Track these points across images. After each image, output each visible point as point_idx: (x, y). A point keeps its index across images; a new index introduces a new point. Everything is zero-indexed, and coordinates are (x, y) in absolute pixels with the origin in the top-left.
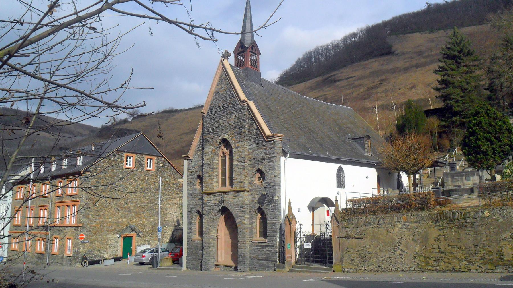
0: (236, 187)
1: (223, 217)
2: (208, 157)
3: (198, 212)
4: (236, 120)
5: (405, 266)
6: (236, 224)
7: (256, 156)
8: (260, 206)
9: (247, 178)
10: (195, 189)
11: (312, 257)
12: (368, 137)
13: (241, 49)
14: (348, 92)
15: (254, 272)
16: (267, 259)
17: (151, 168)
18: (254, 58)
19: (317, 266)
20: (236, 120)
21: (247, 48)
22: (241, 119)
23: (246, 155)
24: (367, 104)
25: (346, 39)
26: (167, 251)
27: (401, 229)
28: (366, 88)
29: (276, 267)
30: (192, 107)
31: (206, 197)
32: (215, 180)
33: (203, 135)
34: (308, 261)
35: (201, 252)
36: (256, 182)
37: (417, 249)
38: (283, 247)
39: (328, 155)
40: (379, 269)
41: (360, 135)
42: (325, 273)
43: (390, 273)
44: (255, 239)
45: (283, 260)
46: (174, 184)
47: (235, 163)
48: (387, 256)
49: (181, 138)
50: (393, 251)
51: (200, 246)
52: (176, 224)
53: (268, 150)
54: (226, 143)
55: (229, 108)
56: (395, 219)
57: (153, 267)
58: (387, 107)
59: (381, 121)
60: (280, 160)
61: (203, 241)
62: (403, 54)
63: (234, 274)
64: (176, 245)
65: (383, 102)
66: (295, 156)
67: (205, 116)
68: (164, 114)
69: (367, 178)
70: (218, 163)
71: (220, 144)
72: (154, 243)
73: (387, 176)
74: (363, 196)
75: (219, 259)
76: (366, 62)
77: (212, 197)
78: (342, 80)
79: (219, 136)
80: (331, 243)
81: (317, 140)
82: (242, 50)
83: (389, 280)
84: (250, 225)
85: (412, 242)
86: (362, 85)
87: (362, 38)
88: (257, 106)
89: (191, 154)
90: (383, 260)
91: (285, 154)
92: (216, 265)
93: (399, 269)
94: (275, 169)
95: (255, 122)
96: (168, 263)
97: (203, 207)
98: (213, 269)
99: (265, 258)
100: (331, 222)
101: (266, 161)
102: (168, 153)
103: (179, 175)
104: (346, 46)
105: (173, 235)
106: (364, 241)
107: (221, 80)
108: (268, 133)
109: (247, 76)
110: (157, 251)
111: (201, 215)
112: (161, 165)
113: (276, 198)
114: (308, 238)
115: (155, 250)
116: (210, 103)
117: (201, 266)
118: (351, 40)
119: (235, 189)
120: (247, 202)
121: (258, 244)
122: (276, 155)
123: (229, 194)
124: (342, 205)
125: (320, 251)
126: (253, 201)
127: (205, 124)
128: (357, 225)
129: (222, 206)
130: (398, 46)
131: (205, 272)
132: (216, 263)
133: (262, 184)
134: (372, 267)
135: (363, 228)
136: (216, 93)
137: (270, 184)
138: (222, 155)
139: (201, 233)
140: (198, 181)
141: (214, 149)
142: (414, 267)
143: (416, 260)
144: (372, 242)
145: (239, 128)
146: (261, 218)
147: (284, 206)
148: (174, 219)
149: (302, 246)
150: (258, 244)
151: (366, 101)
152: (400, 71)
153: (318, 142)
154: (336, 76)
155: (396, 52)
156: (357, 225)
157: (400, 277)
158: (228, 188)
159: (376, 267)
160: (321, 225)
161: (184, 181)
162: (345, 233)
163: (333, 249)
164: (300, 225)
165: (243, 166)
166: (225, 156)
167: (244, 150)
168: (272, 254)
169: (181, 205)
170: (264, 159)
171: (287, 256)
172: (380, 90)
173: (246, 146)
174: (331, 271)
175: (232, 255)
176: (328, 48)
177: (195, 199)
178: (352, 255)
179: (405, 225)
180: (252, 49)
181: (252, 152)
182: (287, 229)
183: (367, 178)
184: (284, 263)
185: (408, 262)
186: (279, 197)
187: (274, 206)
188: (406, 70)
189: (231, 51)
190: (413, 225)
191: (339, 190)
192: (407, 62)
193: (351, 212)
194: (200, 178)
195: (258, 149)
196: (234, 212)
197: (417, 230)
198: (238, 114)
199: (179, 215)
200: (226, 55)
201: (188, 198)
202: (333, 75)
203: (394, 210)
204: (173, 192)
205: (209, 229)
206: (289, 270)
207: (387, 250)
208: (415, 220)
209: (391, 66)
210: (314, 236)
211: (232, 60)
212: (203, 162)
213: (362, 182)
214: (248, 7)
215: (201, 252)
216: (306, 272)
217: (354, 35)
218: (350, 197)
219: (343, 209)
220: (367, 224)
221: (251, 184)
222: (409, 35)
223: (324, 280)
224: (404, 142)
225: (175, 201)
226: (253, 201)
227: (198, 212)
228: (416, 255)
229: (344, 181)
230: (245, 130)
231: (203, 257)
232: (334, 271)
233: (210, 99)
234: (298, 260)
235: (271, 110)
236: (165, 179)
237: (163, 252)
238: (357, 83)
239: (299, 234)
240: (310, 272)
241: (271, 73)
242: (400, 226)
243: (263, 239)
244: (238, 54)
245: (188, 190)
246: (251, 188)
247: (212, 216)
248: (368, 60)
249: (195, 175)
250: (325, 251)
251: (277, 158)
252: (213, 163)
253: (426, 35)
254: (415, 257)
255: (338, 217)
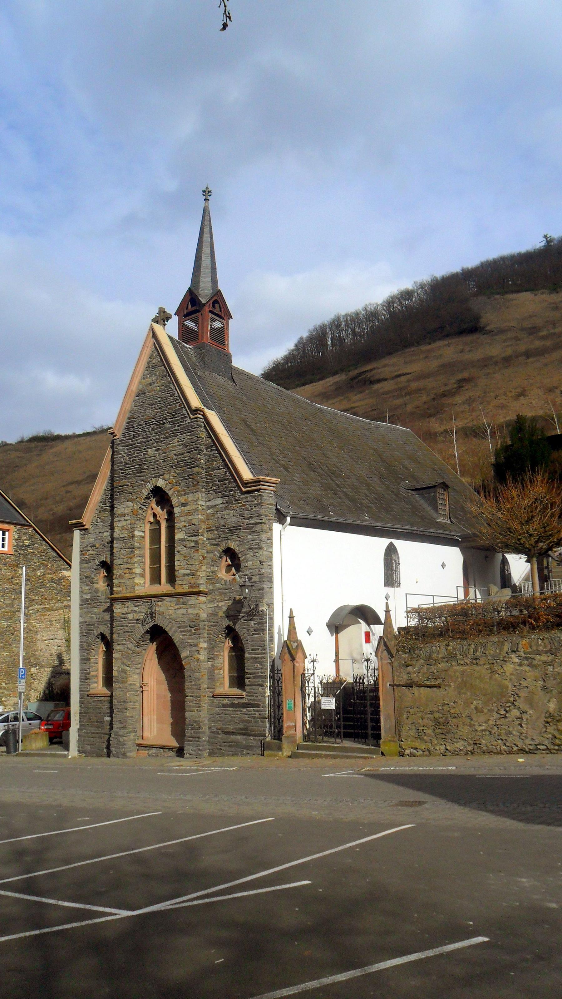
0: (182, 586)
1: (153, 646)
2: (124, 523)
3: (103, 637)
4: (180, 449)
5: (528, 741)
6: (181, 661)
7: (222, 522)
8: (231, 624)
9: (204, 568)
10: (97, 591)
11: (338, 727)
12: (445, 486)
13: (192, 305)
14: (398, 402)
15: (219, 760)
16: (245, 732)
17: (6, 549)
18: (217, 324)
19: (347, 744)
20: (180, 449)
21: (204, 305)
22: (192, 448)
23: (201, 521)
24: (436, 426)
25: (393, 302)
26: (36, 717)
27: (515, 664)
28: (432, 396)
29: (264, 747)
30: (90, 430)
31: (118, 607)
32: (138, 570)
33: (112, 479)
34: (331, 734)
35: (109, 719)
36: (223, 574)
37: (552, 706)
38: (277, 705)
39: (366, 520)
40: (476, 749)
41: (428, 483)
42: (365, 758)
43: (499, 756)
44: (219, 690)
45: (278, 734)
46: (53, 581)
47: (179, 536)
48: (491, 722)
49: (68, 492)
50: (503, 712)
51: (105, 707)
52: (56, 663)
53: (247, 509)
54: (161, 496)
55: (167, 426)
56: (507, 647)
57: (8, 752)
58: (473, 433)
59: (462, 457)
60: (271, 530)
61: (112, 696)
62: (501, 331)
63: (176, 763)
64: (56, 706)
65: (466, 421)
66: (298, 522)
67: (117, 442)
68: (33, 445)
69: (443, 566)
70: (143, 537)
71: (148, 498)
72: (11, 702)
73: (481, 562)
74: (440, 601)
75: (146, 734)
76: (433, 346)
77: (131, 606)
78: (385, 380)
79: (145, 481)
80: (377, 698)
81: (345, 490)
82: (194, 308)
83: (498, 772)
84: (209, 663)
85: (541, 693)
86: (425, 389)
87: (422, 301)
88: (225, 422)
89: (88, 518)
90: (484, 730)
91: (281, 518)
92: (139, 745)
93: (515, 748)
94: (261, 548)
95: (220, 453)
96: (40, 743)
97: (112, 627)
98: (133, 754)
99: (241, 729)
100: (376, 656)
101: (242, 533)
102: (41, 521)
103: (62, 562)
104: (393, 315)
105: (49, 684)
106: (445, 692)
107: (151, 367)
108: (247, 474)
109: (203, 360)
110: (16, 719)
111: (108, 643)
112: (26, 543)
113: (264, 608)
114: (329, 688)
115: (11, 715)
116: (128, 415)
117: (108, 747)
118: (401, 303)
119: (179, 590)
120: (204, 616)
121: (226, 701)
122: (264, 519)
123: (168, 599)
124: (400, 621)
125: (355, 714)
126: (215, 614)
127: (118, 458)
128: (429, 660)
129: (151, 624)
130: (491, 318)
131: (116, 760)
132: (140, 741)
133: (234, 580)
134: (460, 745)
135: (443, 665)
136: (141, 393)
137: (250, 579)
138: (152, 520)
139: (109, 681)
140: (103, 573)
141: (136, 507)
142: (546, 742)
143: (551, 729)
144: (460, 693)
145: (186, 466)
146: (232, 649)
147: (280, 623)
148: (53, 651)
149: (315, 706)
150: (226, 701)
151: (433, 419)
152: (496, 363)
153: (345, 494)
154: (373, 372)
155: (488, 328)
156: (429, 660)
157: (521, 764)
158: (164, 587)
159: (469, 744)
160: (354, 661)
161: (73, 575)
162: (405, 677)
163: (382, 708)
164: (313, 661)
165: (196, 542)
166: (158, 523)
167: (197, 510)
168: (256, 722)
169: (66, 624)
170: (239, 527)
171: (285, 725)
172: (458, 399)
173: (201, 503)
174: (377, 754)
175: (172, 724)
176: (359, 319)
177: (96, 610)
178: (420, 721)
179: (527, 658)
180: (214, 307)
181: (213, 515)
182: (286, 670)
183: (443, 566)
184: (280, 739)
185: (534, 733)
186: (270, 605)
187: (259, 623)
188: (507, 361)
189: (172, 309)
190: (544, 658)
191: (390, 590)
192: (508, 346)
193: (417, 634)
194: (107, 567)
195: (226, 509)
196: (177, 637)
197: (550, 668)
198: (186, 436)
199: (63, 643)
200: (162, 318)
201: (81, 609)
202: (367, 371)
203: (504, 629)
204: (49, 598)
205: (124, 671)
206: (290, 753)
207: (491, 711)
208: (548, 648)
209: (476, 355)
210: (341, 682)
211: (173, 327)
212: (112, 535)
213: (434, 575)
214: (206, 223)
215: (109, 719)
216: (327, 756)
217: (407, 294)
218: (414, 603)
219: (400, 629)
220: (451, 657)
221: (211, 579)
222: (514, 296)
223: (366, 775)
224: (522, 495)
225: (55, 615)
226: (216, 614)
227: (103, 637)
228: (551, 719)
229: (398, 572)
230: (200, 469)
231: (111, 728)
232: (383, 754)
233: (128, 407)
234: (309, 733)
235: (252, 430)
236: (34, 570)
237: (29, 719)
238: (414, 385)
239: (311, 680)
240: (335, 757)
241: (255, 353)
242: (517, 660)
243: (236, 691)
244: (185, 316)
245: (81, 592)
246: (211, 587)
247: (130, 645)
248: (434, 341)
249: (97, 562)
250: (365, 713)
251: (265, 527)
252: (133, 537)
253: (544, 296)
254: (547, 722)
255: (392, 644)
